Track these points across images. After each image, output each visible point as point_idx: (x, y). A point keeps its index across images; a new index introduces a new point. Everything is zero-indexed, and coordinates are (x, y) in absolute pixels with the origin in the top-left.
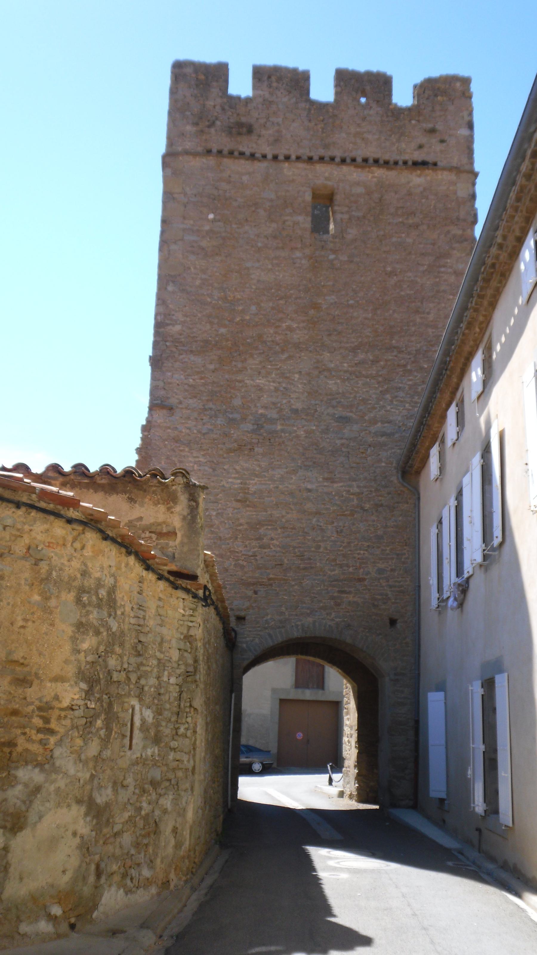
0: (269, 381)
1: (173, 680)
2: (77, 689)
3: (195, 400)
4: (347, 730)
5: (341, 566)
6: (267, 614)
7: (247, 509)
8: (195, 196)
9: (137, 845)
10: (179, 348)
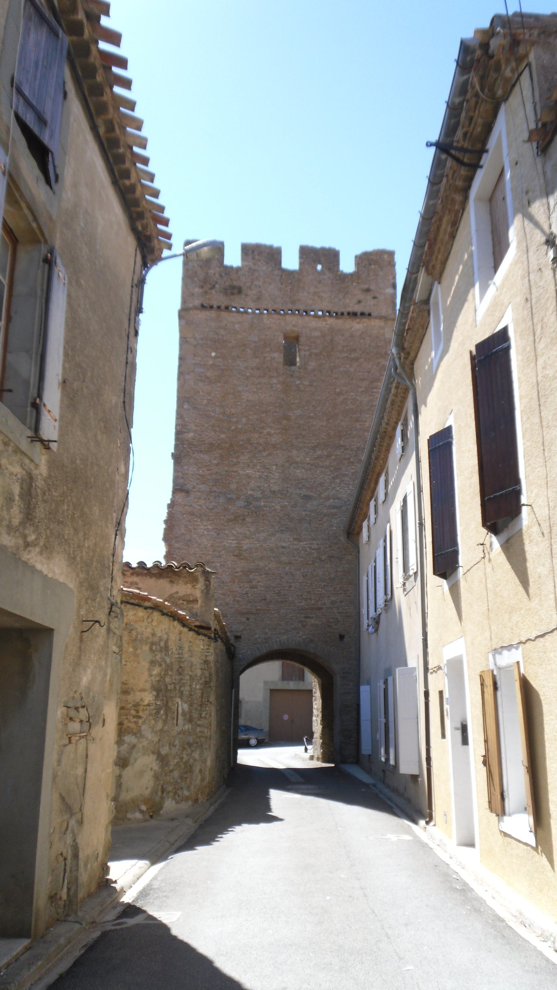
0: (255, 472)
1: (198, 687)
2: (151, 695)
3: (204, 485)
4: (315, 712)
5: (306, 600)
6: (256, 634)
7: (242, 561)
8: (202, 339)
9: (181, 777)
10: (193, 449)
